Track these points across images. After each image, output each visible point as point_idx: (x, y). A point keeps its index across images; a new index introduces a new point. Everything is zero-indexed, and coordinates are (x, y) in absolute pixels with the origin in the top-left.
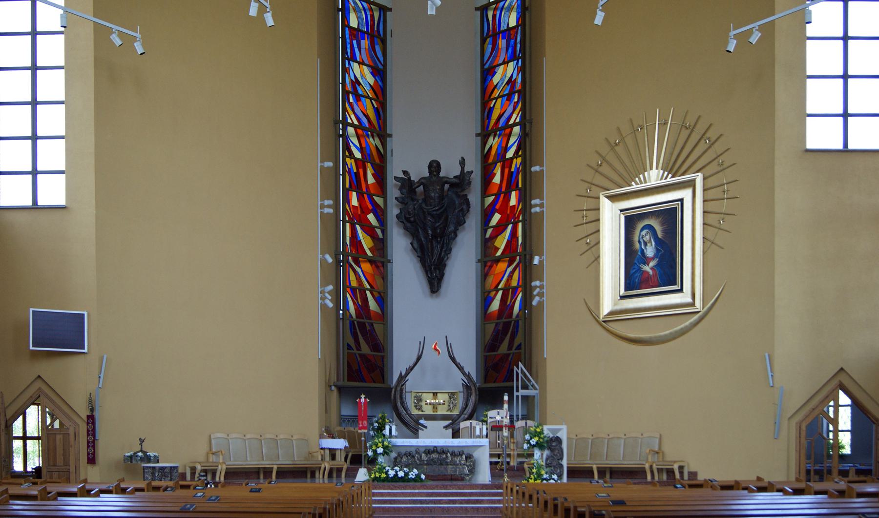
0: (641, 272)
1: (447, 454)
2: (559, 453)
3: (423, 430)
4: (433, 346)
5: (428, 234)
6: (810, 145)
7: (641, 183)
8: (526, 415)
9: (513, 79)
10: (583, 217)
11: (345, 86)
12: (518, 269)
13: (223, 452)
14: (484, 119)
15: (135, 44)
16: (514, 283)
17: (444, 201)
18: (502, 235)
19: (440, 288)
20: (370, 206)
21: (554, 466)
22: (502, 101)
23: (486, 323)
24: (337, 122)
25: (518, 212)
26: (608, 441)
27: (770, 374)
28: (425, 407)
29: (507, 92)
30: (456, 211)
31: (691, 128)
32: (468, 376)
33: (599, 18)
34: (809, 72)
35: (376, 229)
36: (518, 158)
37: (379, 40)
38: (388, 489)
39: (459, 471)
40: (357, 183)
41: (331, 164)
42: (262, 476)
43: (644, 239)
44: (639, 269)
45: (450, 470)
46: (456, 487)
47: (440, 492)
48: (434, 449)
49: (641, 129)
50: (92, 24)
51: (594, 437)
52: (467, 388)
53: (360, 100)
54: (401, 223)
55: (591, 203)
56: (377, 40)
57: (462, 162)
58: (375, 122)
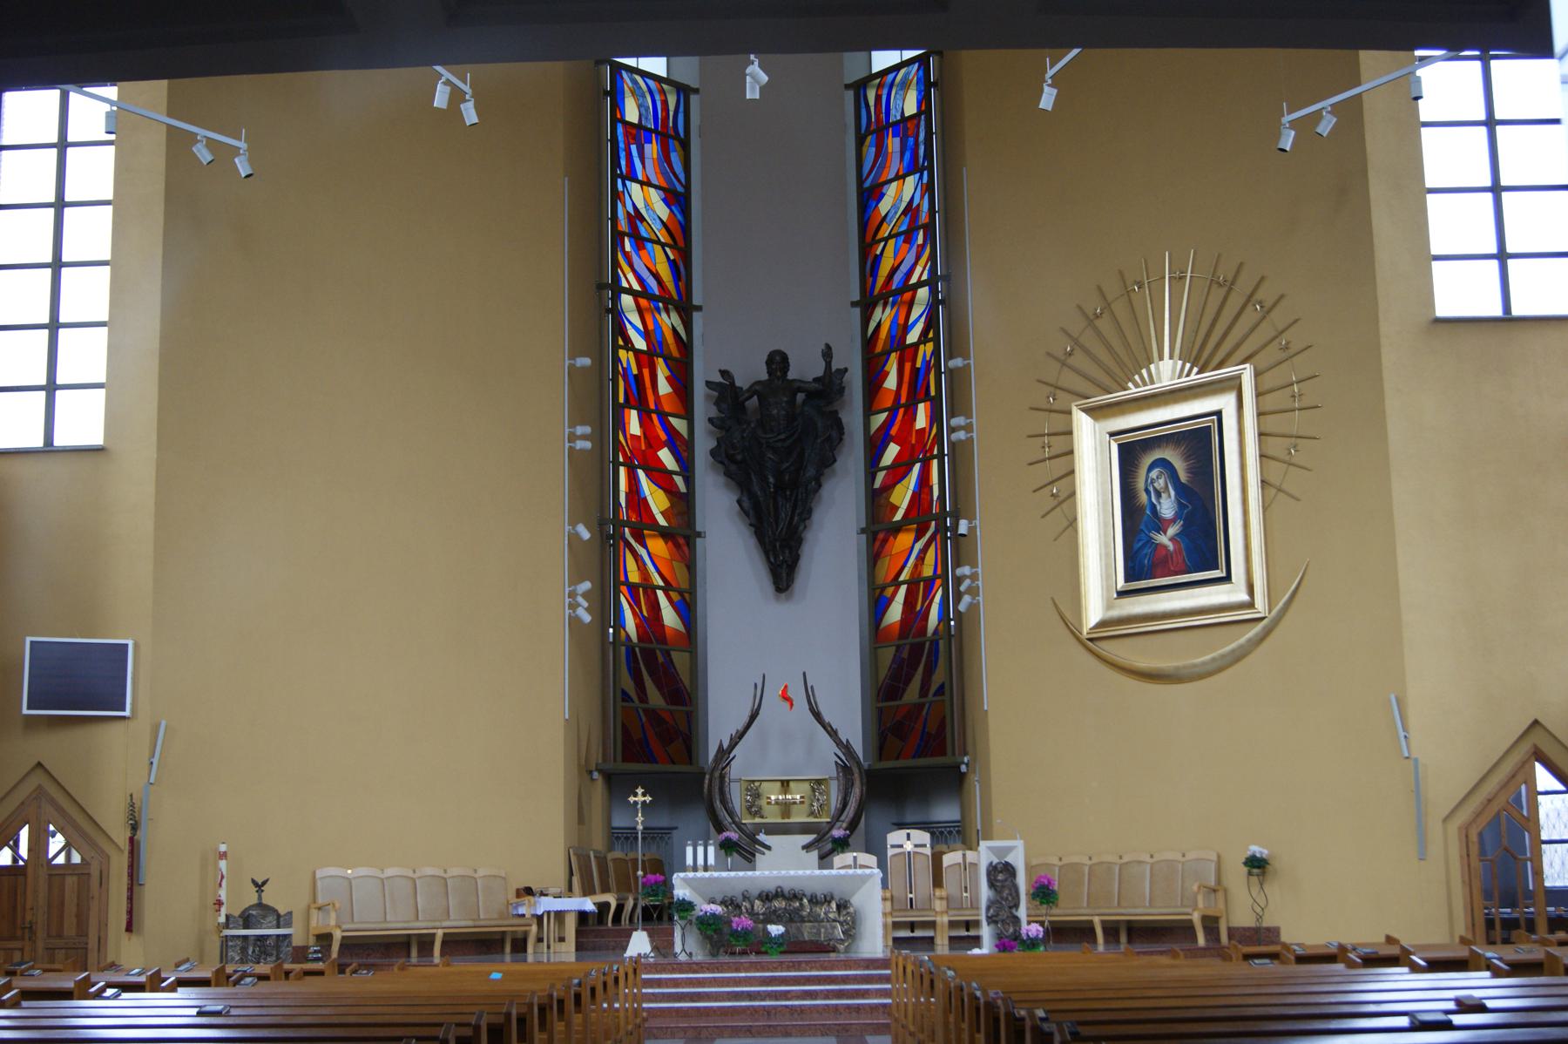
0: (1154, 546)
1: (801, 899)
2: (1011, 895)
3: (764, 854)
4: (780, 692)
5: (768, 483)
6: (1442, 310)
7: (1145, 384)
8: (958, 822)
9: (915, 205)
10: (1044, 447)
11: (617, 224)
12: (933, 545)
13: (337, 905)
14: (865, 275)
15: (237, 160)
16: (928, 571)
17: (795, 424)
18: (903, 482)
19: (793, 582)
20: (663, 436)
21: (1003, 921)
22: (896, 243)
23: (878, 645)
24: (601, 287)
25: (930, 441)
26: (1120, 870)
27: (1402, 734)
28: (766, 809)
29: (904, 228)
30: (819, 441)
31: (1228, 284)
32: (846, 748)
33: (1048, 99)
34: (1429, 184)
35: (674, 476)
36: (927, 344)
37: (676, 143)
38: (687, 972)
39: (825, 933)
40: (639, 396)
41: (585, 361)
42: (414, 952)
43: (1155, 485)
44: (1148, 542)
45: (807, 932)
46: (818, 965)
47: (786, 976)
48: (777, 891)
49: (1139, 288)
50: (164, 128)
51: (1095, 860)
52: (845, 770)
53: (644, 248)
54: (720, 465)
55: (1057, 422)
56: (674, 144)
57: (827, 353)
58: (670, 286)
